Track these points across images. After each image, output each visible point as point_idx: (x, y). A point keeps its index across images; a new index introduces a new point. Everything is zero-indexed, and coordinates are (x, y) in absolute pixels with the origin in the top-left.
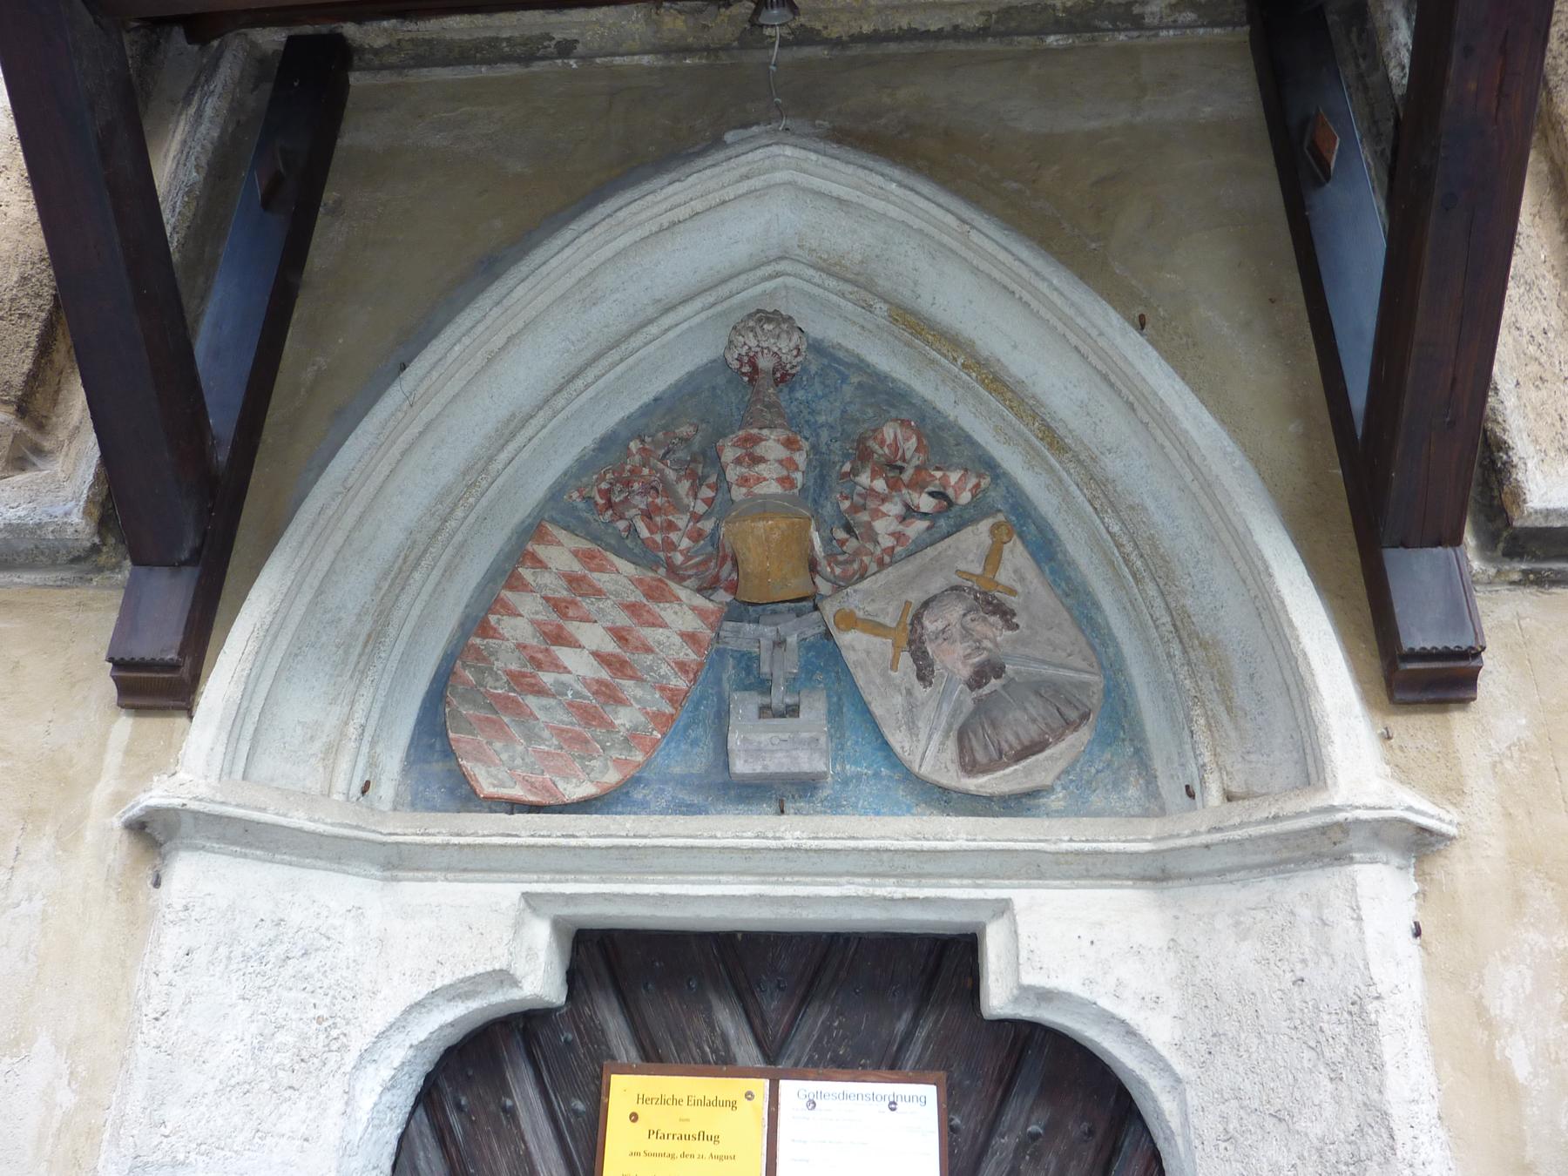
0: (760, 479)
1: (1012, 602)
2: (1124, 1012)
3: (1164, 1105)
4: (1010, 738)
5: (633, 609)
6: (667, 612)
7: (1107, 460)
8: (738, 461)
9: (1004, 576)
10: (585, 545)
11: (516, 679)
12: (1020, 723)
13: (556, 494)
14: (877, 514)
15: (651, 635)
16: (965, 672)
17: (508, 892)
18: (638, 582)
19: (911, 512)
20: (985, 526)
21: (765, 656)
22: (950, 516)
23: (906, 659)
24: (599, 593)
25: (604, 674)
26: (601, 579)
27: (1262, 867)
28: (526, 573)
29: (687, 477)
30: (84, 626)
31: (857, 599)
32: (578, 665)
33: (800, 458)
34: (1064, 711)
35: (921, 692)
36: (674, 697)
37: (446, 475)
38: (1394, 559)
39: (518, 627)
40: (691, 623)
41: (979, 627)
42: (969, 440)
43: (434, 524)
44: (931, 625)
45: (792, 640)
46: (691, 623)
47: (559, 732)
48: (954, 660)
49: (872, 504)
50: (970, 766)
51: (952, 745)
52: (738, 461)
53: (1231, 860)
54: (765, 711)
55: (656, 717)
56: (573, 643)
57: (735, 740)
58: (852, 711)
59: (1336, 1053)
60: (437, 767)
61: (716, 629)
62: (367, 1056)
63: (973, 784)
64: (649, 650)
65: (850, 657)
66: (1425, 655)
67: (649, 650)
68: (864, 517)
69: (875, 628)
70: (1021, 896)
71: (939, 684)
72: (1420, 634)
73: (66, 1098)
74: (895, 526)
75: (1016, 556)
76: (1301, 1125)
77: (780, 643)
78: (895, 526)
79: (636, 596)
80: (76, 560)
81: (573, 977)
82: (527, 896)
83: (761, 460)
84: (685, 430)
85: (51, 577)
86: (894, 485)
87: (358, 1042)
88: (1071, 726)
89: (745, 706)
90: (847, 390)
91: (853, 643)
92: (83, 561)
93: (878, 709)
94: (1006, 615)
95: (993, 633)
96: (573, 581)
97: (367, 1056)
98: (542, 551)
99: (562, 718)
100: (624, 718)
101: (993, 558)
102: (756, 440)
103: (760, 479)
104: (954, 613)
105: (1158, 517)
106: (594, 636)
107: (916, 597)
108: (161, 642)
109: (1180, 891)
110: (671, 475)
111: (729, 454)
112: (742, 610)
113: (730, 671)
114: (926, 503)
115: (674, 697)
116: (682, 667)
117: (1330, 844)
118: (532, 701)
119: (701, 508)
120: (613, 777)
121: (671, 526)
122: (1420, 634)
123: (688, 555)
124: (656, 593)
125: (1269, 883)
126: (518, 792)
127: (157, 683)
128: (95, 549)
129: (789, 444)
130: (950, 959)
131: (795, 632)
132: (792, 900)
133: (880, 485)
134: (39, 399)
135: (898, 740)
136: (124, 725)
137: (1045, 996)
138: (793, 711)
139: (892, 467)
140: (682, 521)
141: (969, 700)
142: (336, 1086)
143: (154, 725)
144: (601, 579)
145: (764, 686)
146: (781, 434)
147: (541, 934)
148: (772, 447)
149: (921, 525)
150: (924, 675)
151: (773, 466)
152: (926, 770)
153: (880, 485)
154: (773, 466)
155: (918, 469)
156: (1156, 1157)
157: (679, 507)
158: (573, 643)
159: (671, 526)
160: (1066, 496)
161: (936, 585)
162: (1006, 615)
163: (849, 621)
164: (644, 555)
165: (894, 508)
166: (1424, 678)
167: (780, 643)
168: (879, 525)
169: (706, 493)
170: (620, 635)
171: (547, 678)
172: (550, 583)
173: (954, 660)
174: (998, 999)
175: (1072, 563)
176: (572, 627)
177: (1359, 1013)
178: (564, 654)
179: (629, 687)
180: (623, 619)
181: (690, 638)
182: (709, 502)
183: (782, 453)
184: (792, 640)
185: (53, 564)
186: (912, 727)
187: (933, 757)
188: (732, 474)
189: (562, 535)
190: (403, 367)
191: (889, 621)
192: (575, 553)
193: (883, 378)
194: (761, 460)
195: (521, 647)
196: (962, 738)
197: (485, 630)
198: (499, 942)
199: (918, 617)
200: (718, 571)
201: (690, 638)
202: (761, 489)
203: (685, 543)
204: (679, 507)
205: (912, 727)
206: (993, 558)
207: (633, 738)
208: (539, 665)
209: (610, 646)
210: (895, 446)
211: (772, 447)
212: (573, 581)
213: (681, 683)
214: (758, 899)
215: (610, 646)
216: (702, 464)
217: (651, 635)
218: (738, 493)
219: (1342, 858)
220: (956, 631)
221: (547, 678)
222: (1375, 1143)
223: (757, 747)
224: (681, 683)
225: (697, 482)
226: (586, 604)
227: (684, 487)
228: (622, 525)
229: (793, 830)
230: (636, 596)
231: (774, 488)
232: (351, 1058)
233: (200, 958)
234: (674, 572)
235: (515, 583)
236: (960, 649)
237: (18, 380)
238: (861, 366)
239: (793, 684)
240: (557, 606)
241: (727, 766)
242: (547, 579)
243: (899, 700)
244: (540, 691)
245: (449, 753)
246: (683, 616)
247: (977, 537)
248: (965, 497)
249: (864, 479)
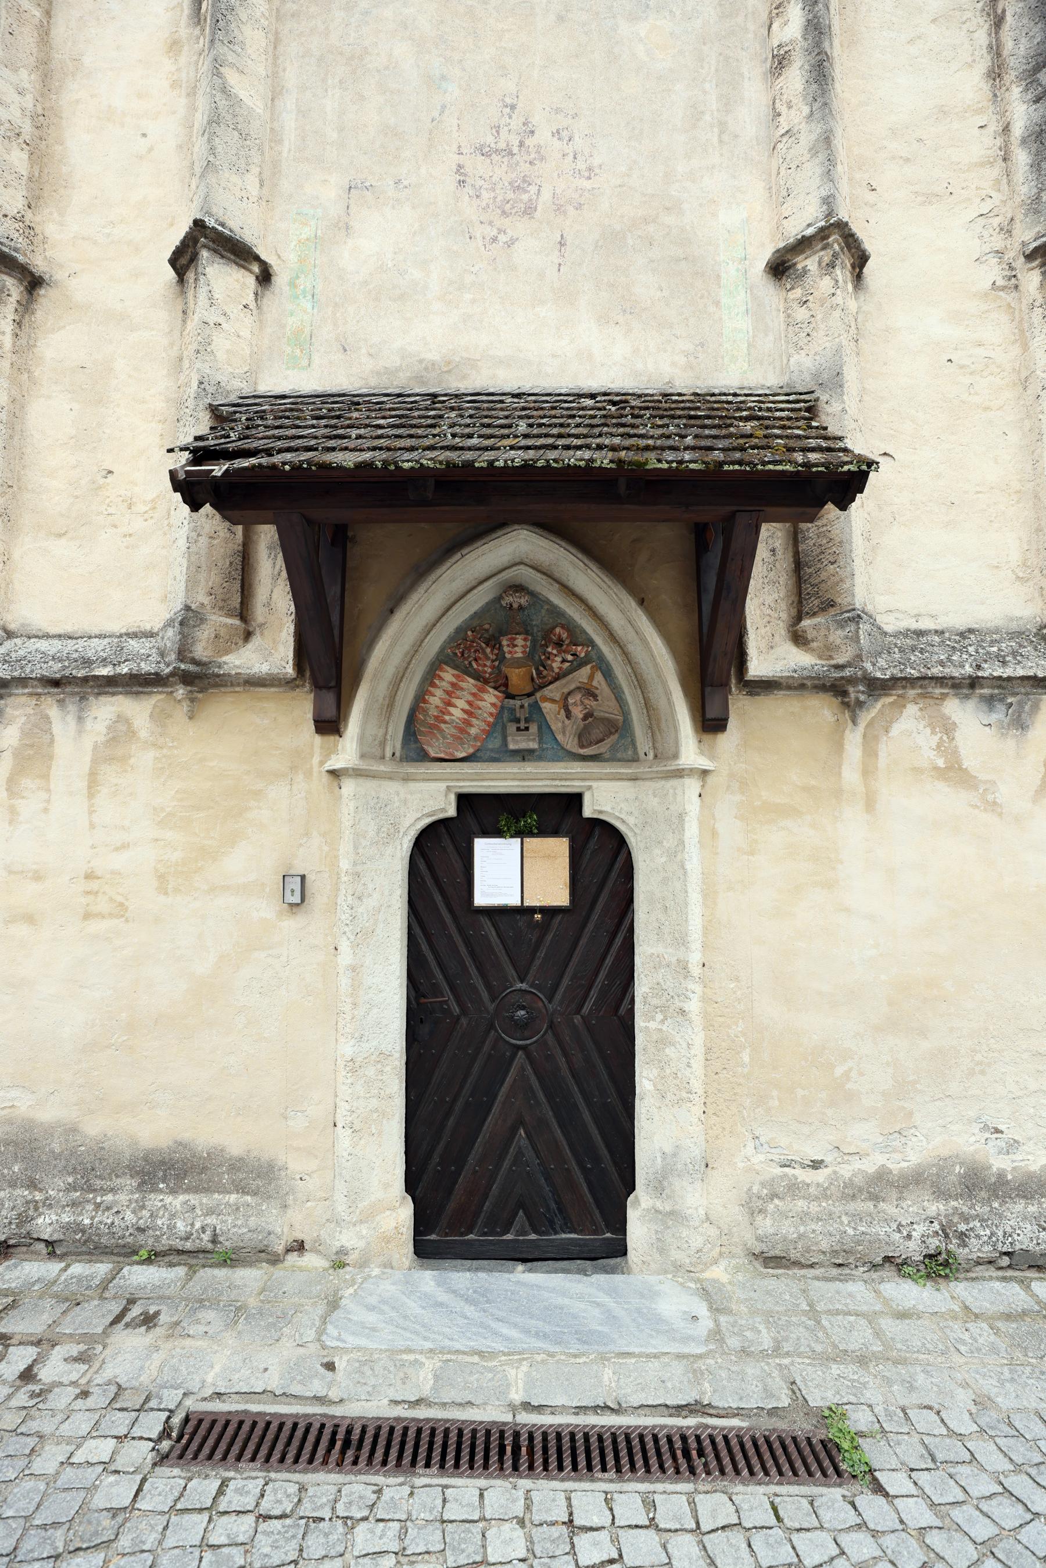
0: (516, 652)
1: (597, 692)
2: (622, 816)
3: (633, 841)
4: (594, 737)
5: (474, 695)
6: (486, 696)
7: (629, 646)
8: (508, 646)
9: (595, 683)
10: (456, 672)
11: (436, 718)
12: (596, 733)
13: (442, 650)
14: (553, 661)
15: (481, 704)
16: (581, 716)
17: (442, 786)
18: (475, 686)
19: (564, 661)
20: (589, 667)
21: (518, 710)
22: (579, 663)
23: (562, 711)
24: (462, 689)
25: (466, 717)
26: (463, 684)
27: (662, 778)
28: (437, 682)
29: (772, 1200)
30: (303, 707)
31: (547, 692)
32: (457, 713)
33: (528, 643)
34: (607, 737)
35: (567, 722)
36: (489, 724)
37: (407, 647)
38: (708, 689)
39: (435, 700)
40: (494, 700)
41: (586, 702)
42: (586, 633)
43: (405, 665)
44: (571, 701)
45: (526, 705)
46: (494, 700)
47: (452, 736)
48: (578, 712)
49: (552, 657)
50: (582, 747)
51: (576, 739)
52: (508, 646)
53: (654, 775)
54: (518, 729)
55: (483, 730)
56: (455, 706)
57: (509, 739)
58: (545, 728)
59: (674, 827)
60: (413, 746)
61: (502, 702)
62: (405, 834)
63: (582, 751)
64: (480, 709)
65: (544, 711)
66: (712, 720)
67: (480, 709)
68: (549, 662)
69: (553, 701)
70: (594, 784)
71: (573, 720)
72: (710, 715)
73: (326, 848)
74: (559, 665)
75: (599, 677)
76: (665, 843)
77: (522, 707)
78: (559, 665)
79: (474, 690)
80: (288, 683)
81: (459, 809)
82: (448, 787)
83: (516, 646)
84: (487, 626)
85: (281, 690)
86: (559, 652)
87: (402, 831)
88: (611, 733)
89: (512, 728)
90: (543, 612)
91: (547, 707)
92: (289, 684)
93: (553, 728)
94: (595, 697)
95: (590, 703)
96: (453, 685)
97: (405, 834)
98: (442, 674)
99: (454, 731)
100: (473, 731)
101: (591, 677)
102: (515, 639)
103: (516, 652)
104: (577, 697)
105: (644, 667)
106: (461, 704)
107: (566, 690)
108: (330, 713)
109: (638, 783)
110: (484, 645)
111: (505, 643)
112: (510, 696)
113: (506, 715)
114: (570, 658)
115: (489, 724)
116: (491, 714)
117: (679, 774)
118: (443, 726)
119: (494, 657)
120: (471, 751)
121: (485, 665)
122: (710, 715)
123: (490, 674)
124: (482, 690)
125: (663, 782)
126: (442, 755)
127: (329, 725)
128: (295, 679)
129: (525, 640)
130: (575, 800)
131: (526, 702)
132: (528, 786)
133: (555, 652)
134: (244, 612)
135: (559, 737)
136: (318, 739)
137: (601, 812)
138: (527, 729)
139: (559, 644)
140: (488, 663)
141: (582, 724)
142: (398, 842)
143: (332, 738)
144: (463, 684)
145: (518, 721)
146: (522, 636)
147: (452, 798)
148: (520, 641)
149: (568, 664)
150: (568, 717)
151: (517, 648)
152: (568, 747)
153: (555, 652)
154: (517, 648)
155: (568, 645)
156: (629, 853)
157: (488, 658)
158: (455, 706)
159: (485, 665)
160: (616, 656)
161: (572, 687)
162: (595, 697)
163: (545, 699)
164: (477, 676)
165: (559, 659)
166: (711, 724)
167: (522, 707)
168: (555, 665)
169: (496, 651)
170: (470, 703)
171: (447, 718)
172: (444, 684)
173: (578, 712)
174: (587, 812)
175: (616, 678)
176: (454, 700)
177: (681, 817)
178: (452, 709)
179: (474, 721)
180: (471, 698)
181: (493, 705)
182: (497, 655)
183: (523, 643)
184: (526, 705)
185: (280, 685)
186: (564, 733)
187: (570, 743)
188: (506, 649)
189: (448, 669)
190: (392, 612)
191: (557, 699)
192: (453, 675)
193: (555, 607)
194: (516, 646)
195: (437, 707)
196: (580, 737)
197: (425, 701)
198: (430, 797)
199: (566, 699)
200: (502, 685)
201: (493, 705)
202: (516, 656)
203: (489, 670)
204: (488, 658)
205: (564, 733)
206: (591, 677)
207: (476, 738)
208: (444, 713)
209: (467, 707)
210: (560, 636)
211: (520, 641)
212: (453, 685)
213: (491, 720)
214: (518, 786)
215: (467, 707)
216: (493, 641)
217: (481, 704)
218: (508, 656)
219: (681, 777)
220: (579, 702)
221: (447, 718)
222: (681, 848)
223: (518, 742)
224: (491, 720)
225: (493, 648)
226: (458, 693)
227: (488, 650)
228: (466, 662)
229: (529, 768)
230: (474, 690)
231: (520, 655)
232: (401, 834)
233: (360, 809)
234: (486, 682)
235: (433, 685)
236: (580, 708)
237: (238, 606)
238: (548, 602)
239: (527, 720)
240: (448, 693)
241: (506, 745)
242: (444, 684)
243: (560, 724)
244: (445, 722)
245: (417, 741)
246: (491, 698)
247: (586, 671)
248: (583, 655)
249: (549, 650)
